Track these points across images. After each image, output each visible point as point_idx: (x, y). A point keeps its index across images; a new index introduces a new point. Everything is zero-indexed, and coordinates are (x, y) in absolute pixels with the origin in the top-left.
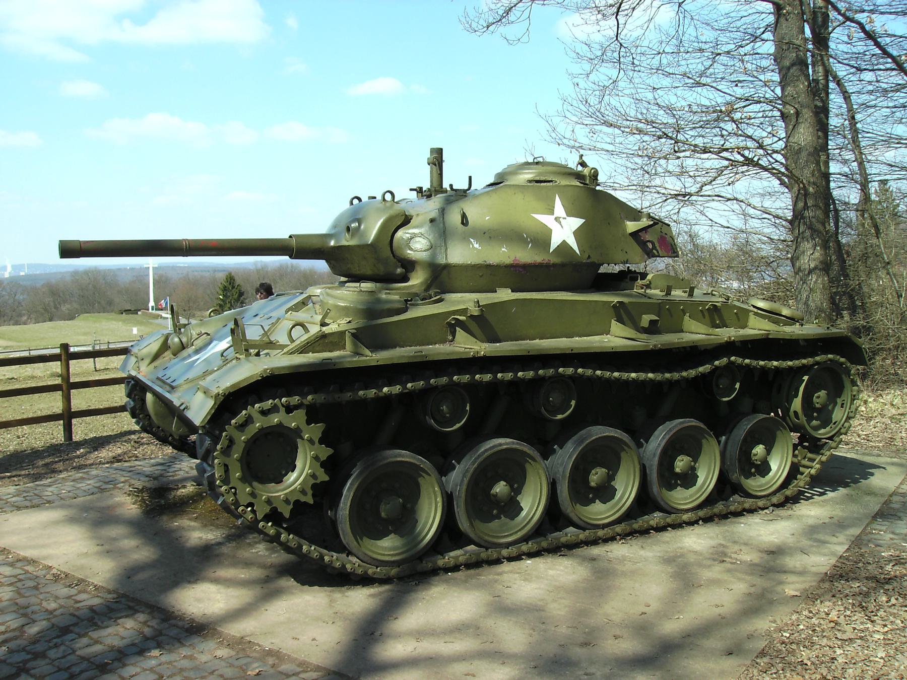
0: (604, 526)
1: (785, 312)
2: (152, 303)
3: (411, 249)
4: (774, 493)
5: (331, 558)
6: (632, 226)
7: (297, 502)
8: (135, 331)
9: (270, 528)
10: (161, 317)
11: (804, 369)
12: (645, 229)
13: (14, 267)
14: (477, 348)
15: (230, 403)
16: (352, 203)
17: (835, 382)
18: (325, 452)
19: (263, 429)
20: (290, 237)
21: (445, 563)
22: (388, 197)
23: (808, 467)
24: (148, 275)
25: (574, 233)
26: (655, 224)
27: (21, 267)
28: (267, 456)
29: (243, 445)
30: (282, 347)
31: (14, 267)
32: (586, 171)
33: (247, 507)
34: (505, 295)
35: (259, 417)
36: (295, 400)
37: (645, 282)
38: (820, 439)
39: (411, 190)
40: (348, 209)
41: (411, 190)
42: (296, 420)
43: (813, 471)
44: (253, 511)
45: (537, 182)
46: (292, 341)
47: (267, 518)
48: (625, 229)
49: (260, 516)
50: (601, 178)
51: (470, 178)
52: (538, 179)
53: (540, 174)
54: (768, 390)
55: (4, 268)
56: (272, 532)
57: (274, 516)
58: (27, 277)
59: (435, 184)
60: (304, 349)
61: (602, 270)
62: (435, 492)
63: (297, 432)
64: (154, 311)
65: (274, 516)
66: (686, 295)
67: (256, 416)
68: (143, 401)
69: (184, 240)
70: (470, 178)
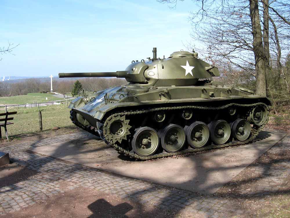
0: (200, 148)
1: (249, 91)
2: (52, 89)
3: (149, 75)
4: (246, 140)
5: (131, 154)
6: (207, 68)
7: (123, 140)
8: (47, 99)
9: (116, 146)
10: (55, 94)
11: (254, 107)
12: (210, 69)
13: (6, 78)
14: (167, 101)
15: (108, 114)
16: (132, 63)
17: (261, 109)
18: (130, 127)
19: (115, 121)
20: (117, 72)
21: (159, 156)
22: (143, 61)
23: (255, 133)
24: (51, 80)
25: (202, 140)
26: (213, 68)
27: (8, 77)
28: (116, 127)
29: (110, 125)
30: (118, 101)
31: (6, 78)
32: (195, 54)
33: (111, 140)
34: (173, 87)
35: (113, 118)
36: (122, 113)
37: (210, 83)
38: (258, 126)
39: (147, 58)
40: (131, 64)
41: (147, 58)
42: (123, 119)
43: (257, 135)
44: (112, 142)
45: (182, 57)
46: (120, 99)
47: (116, 143)
48: (205, 69)
49: (114, 143)
50: (199, 56)
51: (164, 56)
52: (182, 56)
53: (182, 55)
54: (243, 113)
55: (2, 78)
56: (117, 147)
57: (117, 143)
58: (10, 81)
59: (155, 57)
60: (123, 101)
61: (199, 80)
62: (156, 138)
63: (123, 121)
64: (52, 92)
65: (117, 143)
66: (215, 86)
67: (113, 117)
68: (76, 116)
69: (91, 73)
70: (164, 56)
